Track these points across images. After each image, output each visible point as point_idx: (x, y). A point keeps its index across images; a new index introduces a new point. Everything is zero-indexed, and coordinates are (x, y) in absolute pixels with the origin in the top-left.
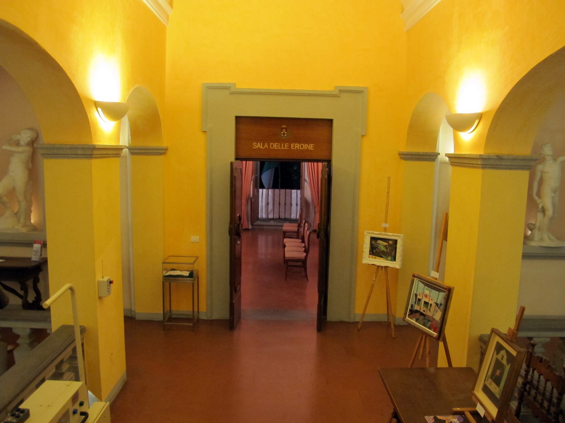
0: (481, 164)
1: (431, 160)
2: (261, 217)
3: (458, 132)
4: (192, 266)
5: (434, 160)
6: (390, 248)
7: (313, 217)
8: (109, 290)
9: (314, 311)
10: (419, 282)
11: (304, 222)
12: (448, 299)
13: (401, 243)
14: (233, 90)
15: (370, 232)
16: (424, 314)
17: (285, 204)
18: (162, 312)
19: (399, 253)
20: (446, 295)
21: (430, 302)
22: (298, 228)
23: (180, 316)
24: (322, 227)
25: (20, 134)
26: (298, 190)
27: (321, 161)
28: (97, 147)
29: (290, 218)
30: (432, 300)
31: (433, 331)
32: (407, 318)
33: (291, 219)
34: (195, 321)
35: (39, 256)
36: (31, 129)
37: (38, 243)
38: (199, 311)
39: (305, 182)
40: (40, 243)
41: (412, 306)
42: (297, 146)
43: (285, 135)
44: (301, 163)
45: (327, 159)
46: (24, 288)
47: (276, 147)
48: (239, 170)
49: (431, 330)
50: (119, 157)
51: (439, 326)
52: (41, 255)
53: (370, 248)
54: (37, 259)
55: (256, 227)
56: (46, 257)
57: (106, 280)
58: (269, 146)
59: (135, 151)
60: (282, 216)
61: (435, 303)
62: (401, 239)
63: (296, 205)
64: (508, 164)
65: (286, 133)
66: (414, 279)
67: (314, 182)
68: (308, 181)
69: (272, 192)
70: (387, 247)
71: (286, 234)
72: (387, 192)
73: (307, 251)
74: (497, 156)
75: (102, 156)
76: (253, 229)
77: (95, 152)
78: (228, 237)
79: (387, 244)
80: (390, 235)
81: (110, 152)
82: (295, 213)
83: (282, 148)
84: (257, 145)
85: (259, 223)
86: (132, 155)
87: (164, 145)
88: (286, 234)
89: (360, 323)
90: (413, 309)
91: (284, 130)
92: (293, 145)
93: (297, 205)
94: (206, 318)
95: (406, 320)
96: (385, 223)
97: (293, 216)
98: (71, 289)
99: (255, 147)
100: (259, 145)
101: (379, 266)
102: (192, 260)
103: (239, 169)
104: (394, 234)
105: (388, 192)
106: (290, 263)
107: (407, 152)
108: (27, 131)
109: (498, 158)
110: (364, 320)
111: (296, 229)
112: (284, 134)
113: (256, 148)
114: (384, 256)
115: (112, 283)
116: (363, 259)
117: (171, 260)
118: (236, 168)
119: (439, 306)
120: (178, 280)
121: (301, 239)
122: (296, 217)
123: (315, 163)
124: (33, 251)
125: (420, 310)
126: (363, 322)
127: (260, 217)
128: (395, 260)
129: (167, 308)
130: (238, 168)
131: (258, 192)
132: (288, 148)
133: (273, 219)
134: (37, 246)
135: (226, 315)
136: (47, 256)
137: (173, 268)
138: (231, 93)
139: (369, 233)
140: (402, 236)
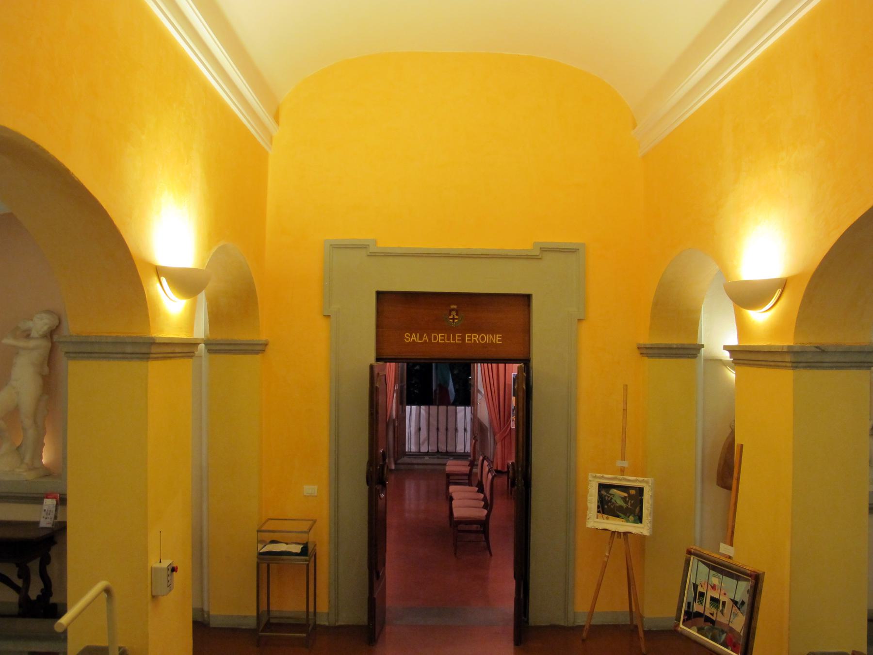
0: (791, 362)
1: (690, 356)
2: (408, 450)
3: (743, 309)
4: (305, 535)
5: (373, 366)
6: (632, 502)
7: (492, 451)
8: (169, 584)
9: (509, 607)
10: (699, 562)
11: (481, 458)
12: (755, 592)
13: (650, 493)
14: (372, 249)
15: (598, 475)
16: (713, 620)
17: (447, 429)
18: (255, 614)
19: (648, 510)
20: (751, 587)
21: (722, 599)
22: (470, 468)
23: (282, 621)
24: (520, 469)
25: (32, 320)
26: (467, 407)
27: (496, 362)
28: (157, 341)
29: (454, 451)
30: (725, 594)
31: (732, 651)
32: (681, 626)
33: (456, 452)
34: (310, 629)
35: (51, 518)
36: (49, 312)
37: (52, 498)
38: (317, 611)
39: (479, 394)
40: (55, 498)
41: (689, 604)
42: (475, 338)
43: (456, 321)
44: (472, 364)
45: (521, 357)
46: (25, 575)
47: (441, 340)
48: (384, 377)
49: (727, 648)
50: (191, 357)
51: (741, 642)
52: (56, 517)
53: (598, 502)
54: (48, 524)
55: (402, 467)
56: (64, 520)
57: (167, 566)
58: (430, 339)
59: (215, 347)
60: (443, 448)
61: (731, 599)
62: (650, 486)
63: (463, 431)
64: (835, 360)
65: (457, 317)
66: (690, 558)
67: (493, 391)
68: (483, 392)
69: (425, 410)
70: (627, 499)
71: (451, 478)
72: (624, 410)
73: (488, 506)
74: (817, 347)
75: (165, 355)
76: (396, 470)
77: (154, 349)
78: (365, 488)
79: (626, 495)
80: (631, 481)
81: (178, 350)
82: (463, 443)
83: (452, 342)
84: (411, 337)
85: (406, 460)
86: (210, 353)
87: (263, 337)
88: (451, 479)
89: (585, 629)
90: (691, 610)
91: (454, 313)
92: (468, 336)
93: (465, 430)
94: (327, 624)
95: (679, 629)
96: (621, 460)
97: (460, 449)
98: (107, 591)
99: (408, 339)
100: (425, 338)
101: (613, 532)
102: (305, 526)
103: (383, 375)
104: (638, 478)
105: (625, 410)
106: (462, 527)
107: (652, 344)
108: (44, 315)
109: (818, 350)
110: (591, 623)
111: (466, 469)
112: (454, 319)
113: (410, 342)
114: (622, 515)
115: (176, 572)
116: (587, 521)
117: (270, 526)
118: (378, 374)
119: (739, 606)
120: (283, 560)
121: (477, 487)
122: (465, 451)
123: (494, 365)
124: (43, 510)
125: (704, 612)
126: (591, 626)
127: (407, 450)
128: (641, 522)
129: (263, 607)
130: (381, 373)
131: (404, 411)
132: (460, 342)
133: (427, 454)
134: (49, 503)
135: (360, 617)
136: (66, 518)
137: (272, 539)
138: (370, 254)
139: (595, 477)
140: (650, 482)
